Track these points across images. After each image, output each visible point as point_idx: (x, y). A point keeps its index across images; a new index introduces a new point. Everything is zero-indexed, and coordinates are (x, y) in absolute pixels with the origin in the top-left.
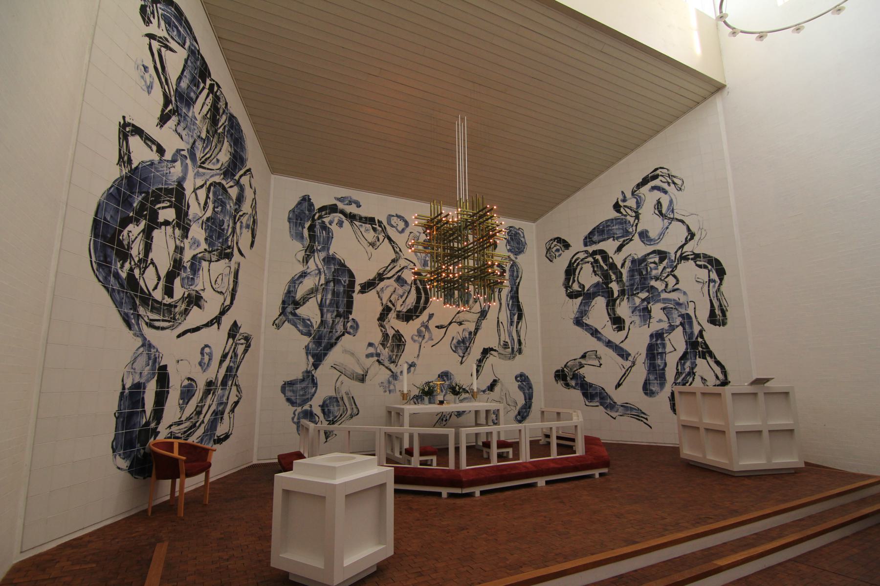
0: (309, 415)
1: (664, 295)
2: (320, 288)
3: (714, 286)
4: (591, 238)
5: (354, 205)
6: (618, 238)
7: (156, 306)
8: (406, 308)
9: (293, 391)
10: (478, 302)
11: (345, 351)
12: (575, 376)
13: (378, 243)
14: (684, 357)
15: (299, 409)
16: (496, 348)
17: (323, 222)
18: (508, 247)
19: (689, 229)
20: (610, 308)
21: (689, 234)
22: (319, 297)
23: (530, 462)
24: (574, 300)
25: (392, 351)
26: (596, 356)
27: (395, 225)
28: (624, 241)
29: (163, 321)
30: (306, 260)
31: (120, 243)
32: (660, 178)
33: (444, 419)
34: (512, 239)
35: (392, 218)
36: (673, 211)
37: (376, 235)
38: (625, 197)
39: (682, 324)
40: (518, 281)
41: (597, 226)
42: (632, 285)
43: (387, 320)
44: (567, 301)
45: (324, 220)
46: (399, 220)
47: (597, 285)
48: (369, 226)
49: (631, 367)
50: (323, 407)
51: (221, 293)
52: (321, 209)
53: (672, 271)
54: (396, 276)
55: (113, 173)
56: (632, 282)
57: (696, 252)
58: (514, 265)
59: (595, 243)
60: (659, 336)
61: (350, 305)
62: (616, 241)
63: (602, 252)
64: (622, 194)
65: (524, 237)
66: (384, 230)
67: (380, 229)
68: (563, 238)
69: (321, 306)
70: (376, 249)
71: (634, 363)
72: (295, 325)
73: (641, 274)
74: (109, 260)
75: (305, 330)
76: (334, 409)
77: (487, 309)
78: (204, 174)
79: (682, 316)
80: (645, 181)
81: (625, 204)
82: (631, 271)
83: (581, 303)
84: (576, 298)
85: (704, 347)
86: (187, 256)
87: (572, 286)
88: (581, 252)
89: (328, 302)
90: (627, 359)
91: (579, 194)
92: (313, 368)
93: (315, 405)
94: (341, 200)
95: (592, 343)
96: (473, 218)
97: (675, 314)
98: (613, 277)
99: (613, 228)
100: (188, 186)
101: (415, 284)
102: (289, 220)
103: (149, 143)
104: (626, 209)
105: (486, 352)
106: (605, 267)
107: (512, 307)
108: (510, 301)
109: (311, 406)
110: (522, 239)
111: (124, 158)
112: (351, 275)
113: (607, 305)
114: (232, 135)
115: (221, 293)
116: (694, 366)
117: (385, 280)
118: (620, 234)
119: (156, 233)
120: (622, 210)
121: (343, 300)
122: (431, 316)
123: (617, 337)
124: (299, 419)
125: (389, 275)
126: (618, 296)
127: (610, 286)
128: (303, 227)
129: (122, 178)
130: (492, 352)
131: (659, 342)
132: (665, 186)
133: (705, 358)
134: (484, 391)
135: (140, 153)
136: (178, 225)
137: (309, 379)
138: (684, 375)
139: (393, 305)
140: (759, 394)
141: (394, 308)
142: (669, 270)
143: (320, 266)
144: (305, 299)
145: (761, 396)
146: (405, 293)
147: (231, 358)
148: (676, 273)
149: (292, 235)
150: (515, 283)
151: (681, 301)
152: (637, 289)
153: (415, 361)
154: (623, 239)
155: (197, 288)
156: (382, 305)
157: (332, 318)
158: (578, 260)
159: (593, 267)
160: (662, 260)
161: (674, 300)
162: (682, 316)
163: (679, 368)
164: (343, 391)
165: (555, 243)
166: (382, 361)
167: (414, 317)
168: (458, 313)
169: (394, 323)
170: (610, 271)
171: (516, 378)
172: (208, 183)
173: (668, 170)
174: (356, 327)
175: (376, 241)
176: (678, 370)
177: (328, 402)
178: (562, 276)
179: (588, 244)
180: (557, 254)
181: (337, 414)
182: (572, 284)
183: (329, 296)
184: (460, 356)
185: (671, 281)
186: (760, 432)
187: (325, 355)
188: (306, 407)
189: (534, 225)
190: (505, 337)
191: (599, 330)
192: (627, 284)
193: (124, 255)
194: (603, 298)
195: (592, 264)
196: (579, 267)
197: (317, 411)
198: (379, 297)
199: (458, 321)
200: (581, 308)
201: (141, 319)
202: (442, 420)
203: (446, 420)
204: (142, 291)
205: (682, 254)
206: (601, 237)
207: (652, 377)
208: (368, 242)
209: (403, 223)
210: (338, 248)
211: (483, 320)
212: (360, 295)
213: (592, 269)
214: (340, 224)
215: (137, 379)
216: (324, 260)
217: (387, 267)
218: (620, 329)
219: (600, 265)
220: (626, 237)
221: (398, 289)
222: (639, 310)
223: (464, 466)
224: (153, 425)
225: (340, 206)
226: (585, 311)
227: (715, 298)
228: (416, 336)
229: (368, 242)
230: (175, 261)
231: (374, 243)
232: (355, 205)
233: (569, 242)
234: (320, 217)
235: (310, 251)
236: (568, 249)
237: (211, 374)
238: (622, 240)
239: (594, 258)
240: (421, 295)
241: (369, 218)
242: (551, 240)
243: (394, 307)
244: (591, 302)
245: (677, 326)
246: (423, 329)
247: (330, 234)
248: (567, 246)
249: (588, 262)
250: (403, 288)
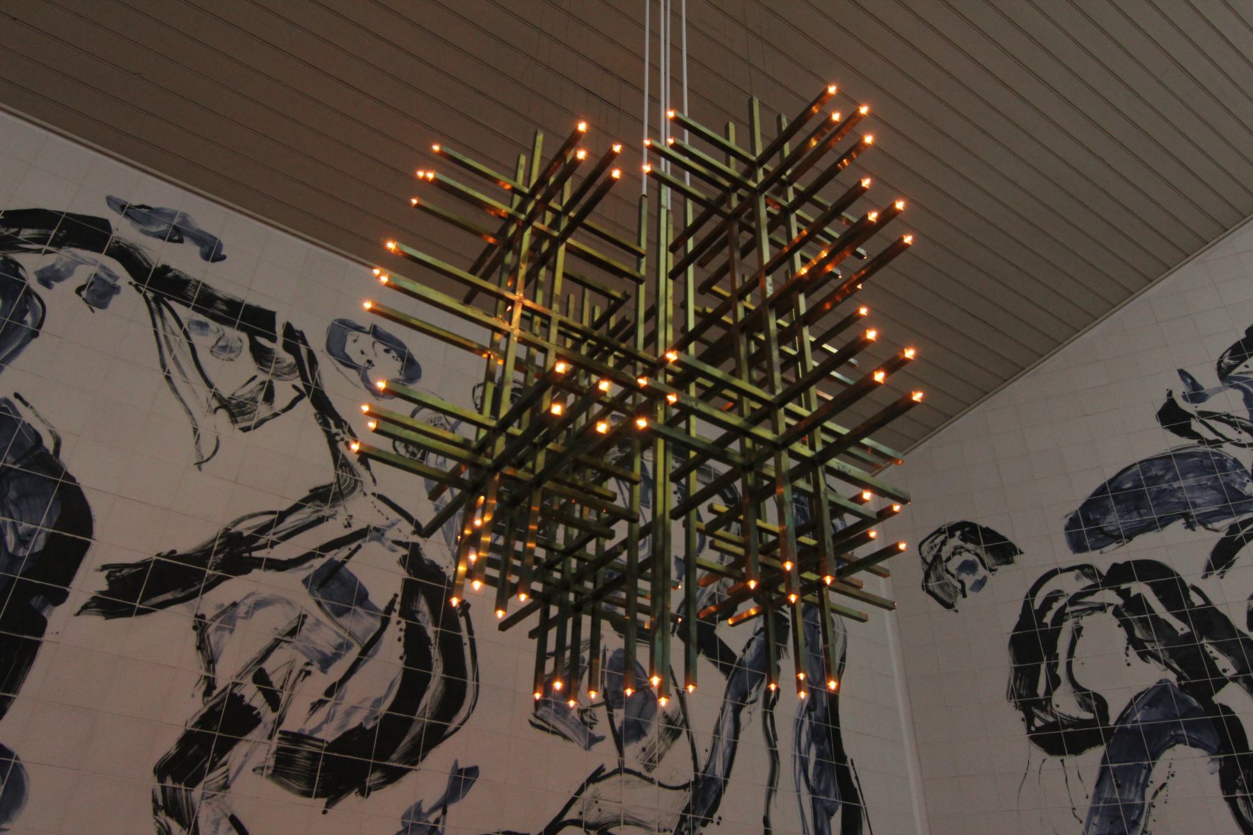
4: (1096, 522)
6: (1205, 520)
8: (336, 722)
10: (684, 735)
13: (263, 410)
20: (1245, 799)
24: (1070, 759)
27: (360, 361)
28: (1233, 529)
35: (352, 335)
37: (263, 377)
38: (1195, 385)
41: (1111, 481)
43: (216, 776)
44: (1035, 765)
45: (19, 257)
46: (380, 347)
47: (1156, 697)
48: (235, 335)
54: (317, 563)
59: (1115, 537)
62: (1200, 528)
63: (1151, 570)
64: (1183, 380)
66: (306, 366)
67: (290, 359)
68: (984, 523)
70: (246, 429)
77: (719, 771)
81: (1203, 407)
83: (1103, 772)
84: (1077, 750)
87: (1049, 701)
88: (1063, 571)
91: (1019, 388)
94: (139, 214)
96: (599, 547)
99: (1176, 485)
101: (408, 612)
104: (1212, 423)
106: (1180, 627)
107: (818, 776)
117: (255, 572)
118: (1210, 503)
120: (1196, 426)
122: (463, 779)
125: (283, 552)
127: (1218, 698)
139: (273, 699)
141: (269, 716)
146: (349, 647)
154: (1230, 521)
156: (207, 693)
158: (1056, 599)
159: (1127, 625)
165: (956, 541)
167: (373, 778)
168: (597, 777)
170: (1204, 641)
175: (254, 400)
178: (1002, 665)
179: (1088, 543)
180: (969, 580)
182: (1049, 692)
194: (1198, 752)
195: (1117, 612)
196: (1067, 627)
198: (202, 646)
199: (592, 817)
200: (1106, 795)
208: (216, 395)
209: (398, 364)
211: (704, 824)
212: (95, 621)
213: (1122, 634)
217: (283, 516)
219: (1156, 619)
220: (1239, 513)
221: (318, 623)
226: (1129, 807)
229: (216, 395)
231: (241, 405)
232: (196, 249)
233: (1011, 538)
236: (1012, 562)
238: (1224, 524)
239: (1124, 594)
240: (430, 667)
241: (248, 307)
242: (939, 532)
243: (275, 709)
244: (1149, 770)
247: (28, 318)
248: (1003, 551)
249: (1102, 608)
250: (341, 620)
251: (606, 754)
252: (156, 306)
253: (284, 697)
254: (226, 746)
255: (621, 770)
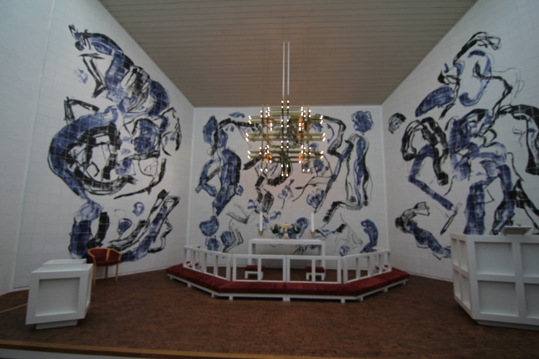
0: (214, 241)
1: (482, 150)
2: (221, 169)
3: (533, 136)
5: (240, 117)
6: (442, 105)
7: (97, 184)
9: (206, 228)
11: (235, 205)
12: (410, 223)
14: (502, 207)
15: (209, 238)
16: (345, 202)
17: (222, 130)
18: (356, 127)
19: (506, 84)
21: (506, 88)
22: (220, 173)
23: (289, 284)
25: (265, 204)
26: (425, 206)
28: (447, 107)
29: (103, 191)
30: (213, 153)
31: (69, 156)
32: (478, 43)
33: (302, 249)
34: (359, 121)
36: (490, 70)
39: (500, 176)
40: (365, 151)
42: (454, 144)
47: (426, 147)
49: (454, 216)
50: (222, 237)
51: (150, 175)
52: (221, 123)
53: (490, 126)
55: (62, 124)
56: (454, 141)
57: (514, 104)
58: (361, 139)
59: (424, 112)
60: (478, 187)
61: (238, 177)
65: (371, 118)
69: (221, 179)
71: (456, 212)
72: (206, 190)
73: (461, 133)
74: (61, 164)
75: (212, 193)
76: (228, 238)
78: (131, 116)
79: (500, 168)
80: (465, 49)
82: (454, 131)
85: (522, 196)
86: (120, 158)
89: (225, 176)
90: (450, 209)
92: (216, 215)
93: (218, 236)
94: (233, 115)
95: (421, 196)
97: (493, 166)
98: (439, 139)
100: (119, 124)
102: (204, 132)
103: (87, 107)
105: (335, 205)
106: (432, 132)
108: (357, 166)
109: (215, 236)
110: (370, 120)
111: (69, 116)
112: (239, 159)
113: (434, 163)
114: (154, 92)
115: (150, 175)
116: (511, 215)
119: (95, 150)
121: (234, 175)
122: (292, 181)
123: (441, 190)
124: (209, 243)
126: (443, 155)
128: (211, 135)
129: (68, 126)
130: (341, 205)
131: (478, 193)
132: (483, 49)
133: (523, 207)
134: (334, 232)
135: (79, 112)
136: (112, 144)
137: (214, 221)
138: (501, 224)
139: (266, 175)
140: (513, 245)
141: (266, 178)
142: (487, 126)
143: (221, 156)
144: (212, 176)
145: (516, 248)
147: (161, 209)
148: (494, 128)
149: (205, 140)
150: (362, 153)
151: (499, 154)
152: (458, 147)
153: (281, 211)
155: (130, 174)
157: (227, 185)
159: (423, 133)
160: (480, 118)
161: (492, 154)
162: (500, 168)
163: (497, 217)
164: (234, 228)
166: (258, 211)
167: (280, 183)
168: (313, 178)
169: (266, 187)
171: (362, 223)
172: (135, 120)
173: (485, 33)
174: (242, 190)
176: (495, 218)
177: (225, 234)
180: (397, 126)
181: (231, 242)
183: (226, 173)
184: (314, 207)
185: (489, 136)
186: (513, 284)
187: (223, 207)
188: (213, 237)
189: (380, 107)
190: (352, 193)
191: (428, 184)
192: (450, 143)
193: (72, 160)
195: (422, 130)
197: (219, 239)
199: (313, 183)
201: (86, 192)
202: (300, 250)
203: (303, 250)
204: (86, 177)
205: (499, 109)
206: (428, 107)
207: (471, 225)
210: (231, 145)
212: (245, 171)
214: (232, 129)
215: (85, 218)
216: (223, 152)
218: (444, 183)
222: (461, 166)
223: (234, 279)
224: (98, 240)
225: (232, 119)
227: (534, 148)
228: (281, 194)
230: (110, 162)
234: (221, 127)
235: (215, 148)
237: (144, 216)
238: (445, 106)
239: (423, 126)
245: (495, 178)
246: (286, 190)
248: (402, 118)
251: (315, 174)
252: (239, 128)
253: (267, 175)
254: (262, 182)
255: (317, 176)
